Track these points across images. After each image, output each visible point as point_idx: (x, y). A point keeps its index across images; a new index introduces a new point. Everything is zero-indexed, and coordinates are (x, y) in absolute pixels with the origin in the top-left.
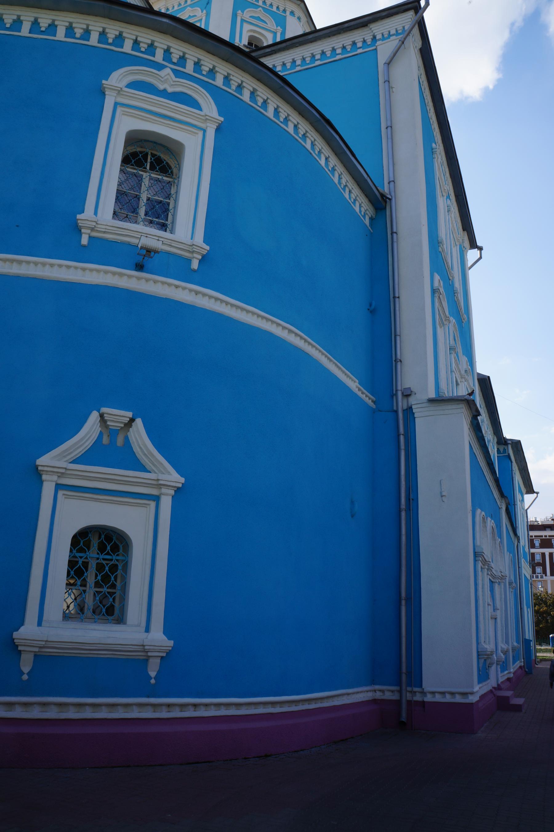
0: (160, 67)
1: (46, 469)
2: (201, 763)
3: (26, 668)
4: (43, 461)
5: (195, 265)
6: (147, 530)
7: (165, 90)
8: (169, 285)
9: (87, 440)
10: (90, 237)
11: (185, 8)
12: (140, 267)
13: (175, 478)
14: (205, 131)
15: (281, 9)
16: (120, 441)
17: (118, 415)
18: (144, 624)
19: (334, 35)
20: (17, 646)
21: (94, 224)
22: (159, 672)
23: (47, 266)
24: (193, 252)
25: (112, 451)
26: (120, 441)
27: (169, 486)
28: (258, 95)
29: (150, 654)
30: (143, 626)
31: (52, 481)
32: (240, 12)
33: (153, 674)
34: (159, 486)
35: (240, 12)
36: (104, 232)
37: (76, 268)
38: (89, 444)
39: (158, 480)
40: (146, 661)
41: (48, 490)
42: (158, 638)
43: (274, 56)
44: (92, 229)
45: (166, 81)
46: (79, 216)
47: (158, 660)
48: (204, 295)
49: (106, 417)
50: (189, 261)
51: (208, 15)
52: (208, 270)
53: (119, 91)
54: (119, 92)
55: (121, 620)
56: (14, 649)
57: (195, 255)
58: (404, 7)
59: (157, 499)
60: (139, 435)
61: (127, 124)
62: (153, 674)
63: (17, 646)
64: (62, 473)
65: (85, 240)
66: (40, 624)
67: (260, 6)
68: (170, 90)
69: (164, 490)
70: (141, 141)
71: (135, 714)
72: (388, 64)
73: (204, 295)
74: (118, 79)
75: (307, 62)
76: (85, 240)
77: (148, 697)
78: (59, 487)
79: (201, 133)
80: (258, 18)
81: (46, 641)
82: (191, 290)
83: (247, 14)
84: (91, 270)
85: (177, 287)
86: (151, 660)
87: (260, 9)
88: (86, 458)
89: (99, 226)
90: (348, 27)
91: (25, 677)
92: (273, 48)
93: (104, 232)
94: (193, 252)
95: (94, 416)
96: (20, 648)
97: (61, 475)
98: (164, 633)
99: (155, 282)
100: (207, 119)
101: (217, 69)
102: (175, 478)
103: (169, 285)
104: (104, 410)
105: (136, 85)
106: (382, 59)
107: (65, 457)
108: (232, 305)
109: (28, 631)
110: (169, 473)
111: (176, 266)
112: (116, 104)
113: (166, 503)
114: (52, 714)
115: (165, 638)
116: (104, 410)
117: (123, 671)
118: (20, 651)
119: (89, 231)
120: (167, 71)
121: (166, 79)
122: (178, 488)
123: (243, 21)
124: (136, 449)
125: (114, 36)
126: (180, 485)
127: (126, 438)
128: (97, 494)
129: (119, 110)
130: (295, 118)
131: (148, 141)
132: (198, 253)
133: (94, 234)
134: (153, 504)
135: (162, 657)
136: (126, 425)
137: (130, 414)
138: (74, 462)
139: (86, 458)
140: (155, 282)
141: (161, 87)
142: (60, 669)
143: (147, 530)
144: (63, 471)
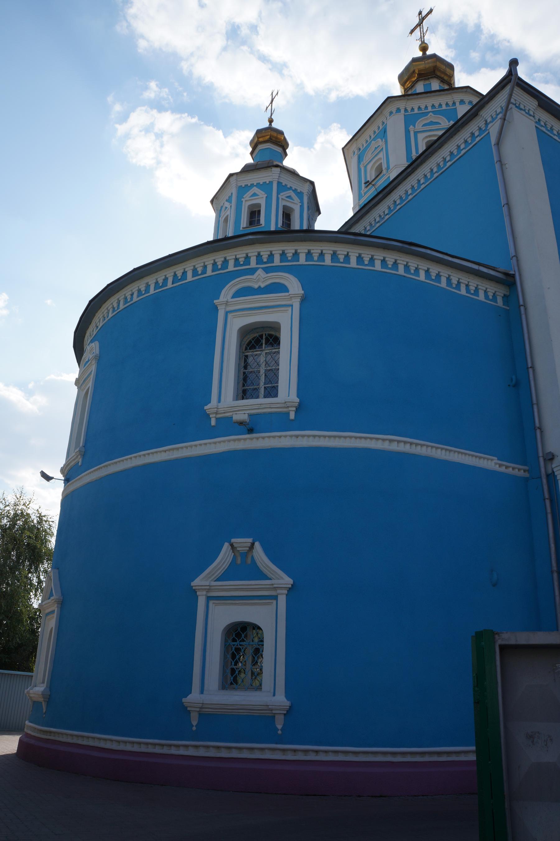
0: (253, 271)
1: (197, 588)
2: (311, 795)
3: (194, 723)
4: (197, 582)
5: (292, 416)
6: (271, 620)
7: (260, 287)
8: (274, 437)
9: (224, 563)
10: (217, 419)
11: (370, 142)
12: (251, 431)
13: (288, 581)
14: (292, 306)
15: (450, 103)
16: (249, 561)
17: (242, 542)
18: (272, 691)
19: (455, 134)
20: (186, 708)
21: (216, 409)
22: (284, 725)
23: (193, 447)
24: (288, 407)
25: (243, 568)
26: (249, 561)
27: (282, 588)
28: (339, 254)
29: (274, 712)
30: (271, 692)
31: (203, 595)
32: (411, 127)
33: (279, 727)
34: (275, 589)
35: (411, 127)
36: (224, 413)
37: (210, 443)
38: (226, 565)
39: (273, 584)
40: (273, 717)
41: (201, 601)
42: (281, 700)
43: (416, 172)
44: (216, 413)
45: (258, 280)
46: (206, 408)
47: (282, 717)
48: (303, 436)
49: (235, 545)
50: (288, 414)
51: (386, 142)
52: (306, 414)
53: (226, 304)
54: (227, 303)
55: (259, 688)
56: (185, 711)
57: (290, 409)
58: (502, 84)
59: (275, 598)
60: (259, 552)
61: (238, 323)
62: (279, 727)
63: (186, 708)
64: (209, 589)
65: (213, 422)
66: (202, 692)
67: (429, 112)
68: (263, 286)
69: (279, 591)
70: (255, 329)
71: (268, 755)
72: (498, 144)
73: (303, 436)
74: (226, 294)
75: (455, 154)
76: (213, 422)
77: (276, 743)
78: (209, 598)
79: (290, 309)
80: (432, 123)
81: (203, 704)
82: (291, 436)
83: (419, 126)
84: (220, 442)
85: (280, 437)
86: (277, 716)
87: (431, 114)
88: (223, 577)
89: (220, 410)
90: (462, 123)
91: (194, 728)
92: (412, 167)
93: (224, 413)
94: (288, 407)
95: (226, 545)
96: (189, 709)
97: (209, 590)
98: (286, 697)
99: (263, 438)
100: (291, 297)
101: (299, 251)
102: (288, 581)
103: (274, 437)
104: (233, 540)
105: (240, 293)
106: (493, 140)
107: (210, 577)
108: (330, 437)
109: (194, 698)
110: (282, 578)
111: (278, 422)
112: (227, 313)
113: (282, 600)
114: (212, 753)
115: (285, 699)
116: (233, 540)
117: (257, 724)
118: (189, 711)
119: (214, 415)
120: (260, 272)
121: (260, 279)
122: (290, 588)
123: (416, 133)
124: (259, 564)
125: (221, 262)
126: (290, 586)
127: (252, 557)
128: (234, 600)
129: (230, 316)
130: (379, 255)
131: (258, 328)
132: (292, 407)
133: (218, 416)
134: (275, 602)
135: (285, 714)
136: (249, 548)
137: (250, 540)
138: (218, 580)
139: (223, 577)
140: (263, 438)
141: (256, 286)
142: (215, 723)
143: (271, 620)
144: (208, 587)
